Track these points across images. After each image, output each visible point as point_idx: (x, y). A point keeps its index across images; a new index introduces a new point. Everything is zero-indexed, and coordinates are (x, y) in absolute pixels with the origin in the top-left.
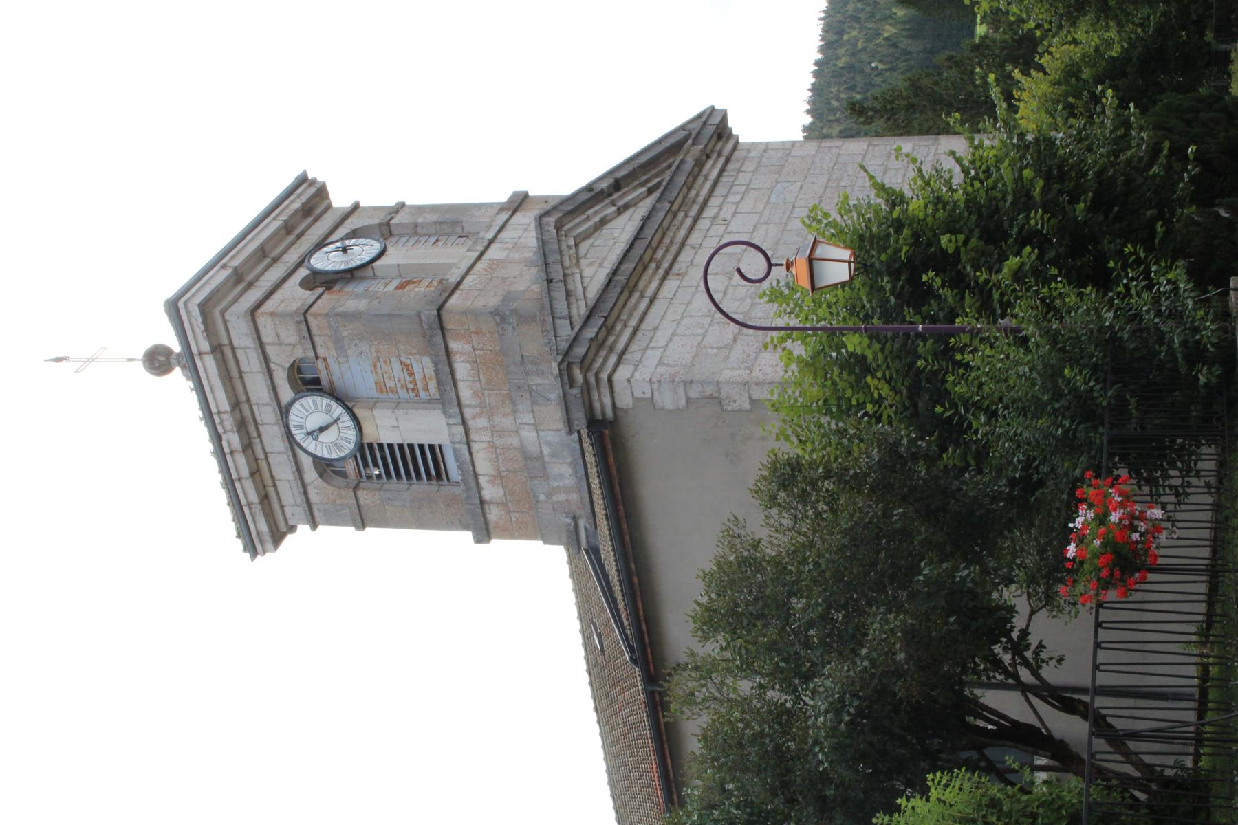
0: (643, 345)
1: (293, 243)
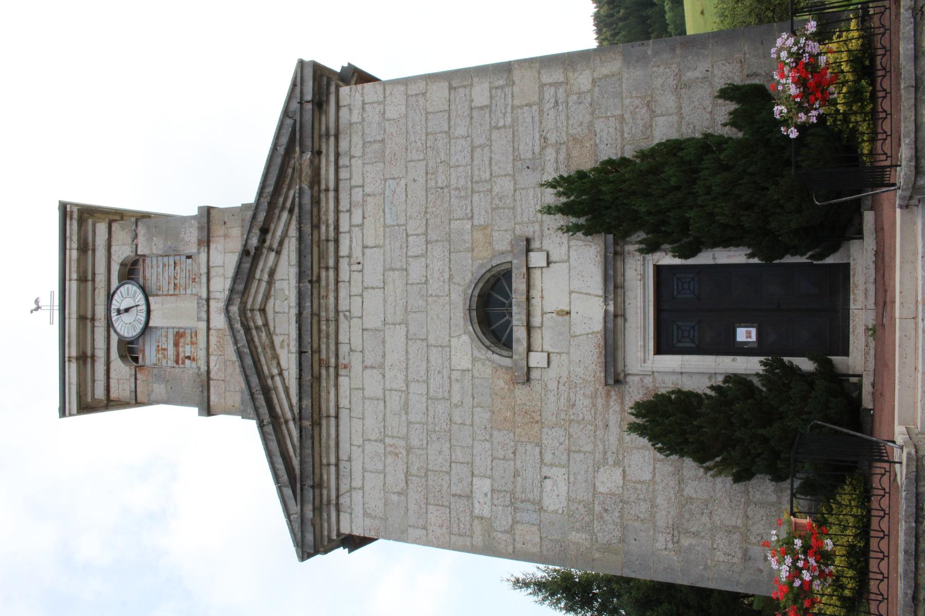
0: (347, 487)
1: (94, 289)
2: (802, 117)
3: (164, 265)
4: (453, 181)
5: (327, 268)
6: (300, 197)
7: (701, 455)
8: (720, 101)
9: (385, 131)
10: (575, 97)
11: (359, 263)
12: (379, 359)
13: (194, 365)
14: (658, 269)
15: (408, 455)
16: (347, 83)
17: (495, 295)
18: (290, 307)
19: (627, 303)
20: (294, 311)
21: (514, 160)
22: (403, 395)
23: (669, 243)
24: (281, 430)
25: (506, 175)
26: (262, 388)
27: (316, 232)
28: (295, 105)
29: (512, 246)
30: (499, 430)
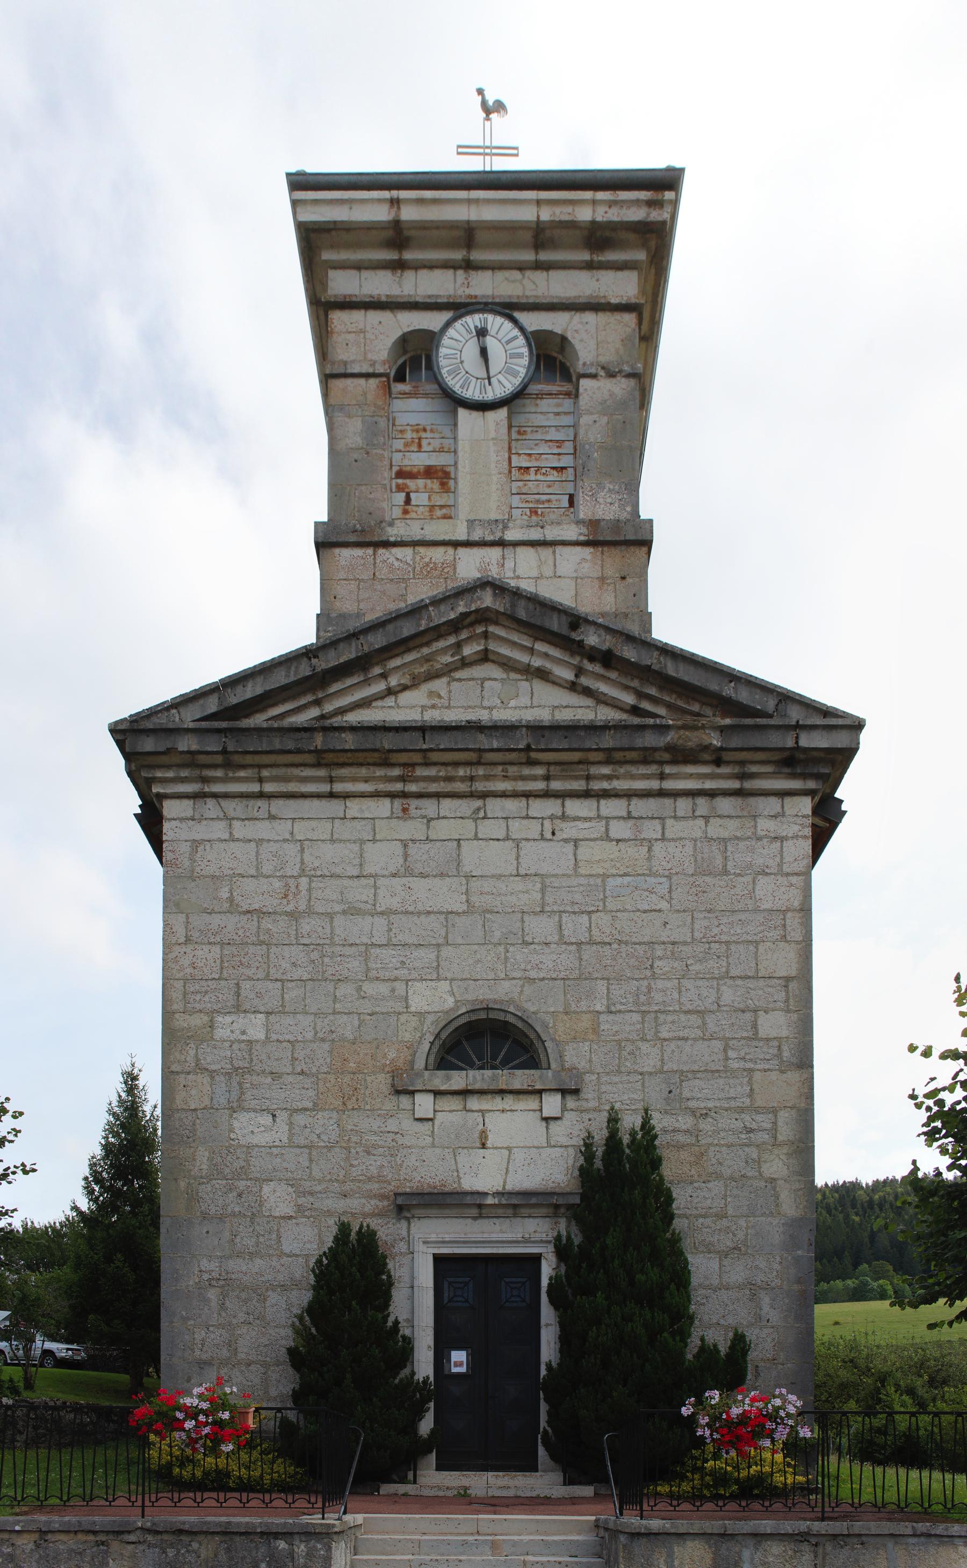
0: (231, 814)
1: (521, 267)
2: (704, 1420)
3: (559, 443)
4: (660, 984)
5: (547, 778)
6: (655, 727)
7: (315, 1310)
8: (731, 1335)
9: (739, 875)
10: (755, 1156)
11: (553, 834)
12: (418, 868)
13: (397, 512)
14: (535, 1260)
15: (287, 914)
16: (816, 811)
17: (507, 1046)
18: (491, 708)
19: (495, 1220)
20: (484, 716)
21: (682, 1072)
22: (369, 906)
23: (566, 1271)
24: (304, 693)
25: (662, 1060)
26: (366, 655)
27: (600, 756)
28: (795, 714)
29: (570, 1070)
30: (331, 1052)
